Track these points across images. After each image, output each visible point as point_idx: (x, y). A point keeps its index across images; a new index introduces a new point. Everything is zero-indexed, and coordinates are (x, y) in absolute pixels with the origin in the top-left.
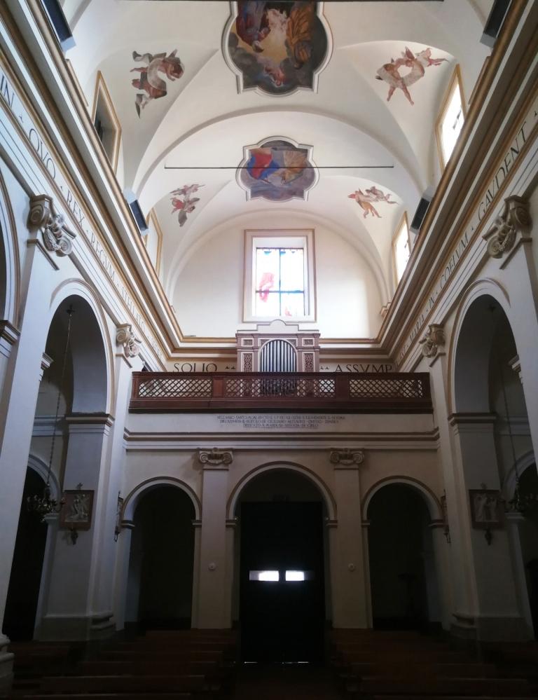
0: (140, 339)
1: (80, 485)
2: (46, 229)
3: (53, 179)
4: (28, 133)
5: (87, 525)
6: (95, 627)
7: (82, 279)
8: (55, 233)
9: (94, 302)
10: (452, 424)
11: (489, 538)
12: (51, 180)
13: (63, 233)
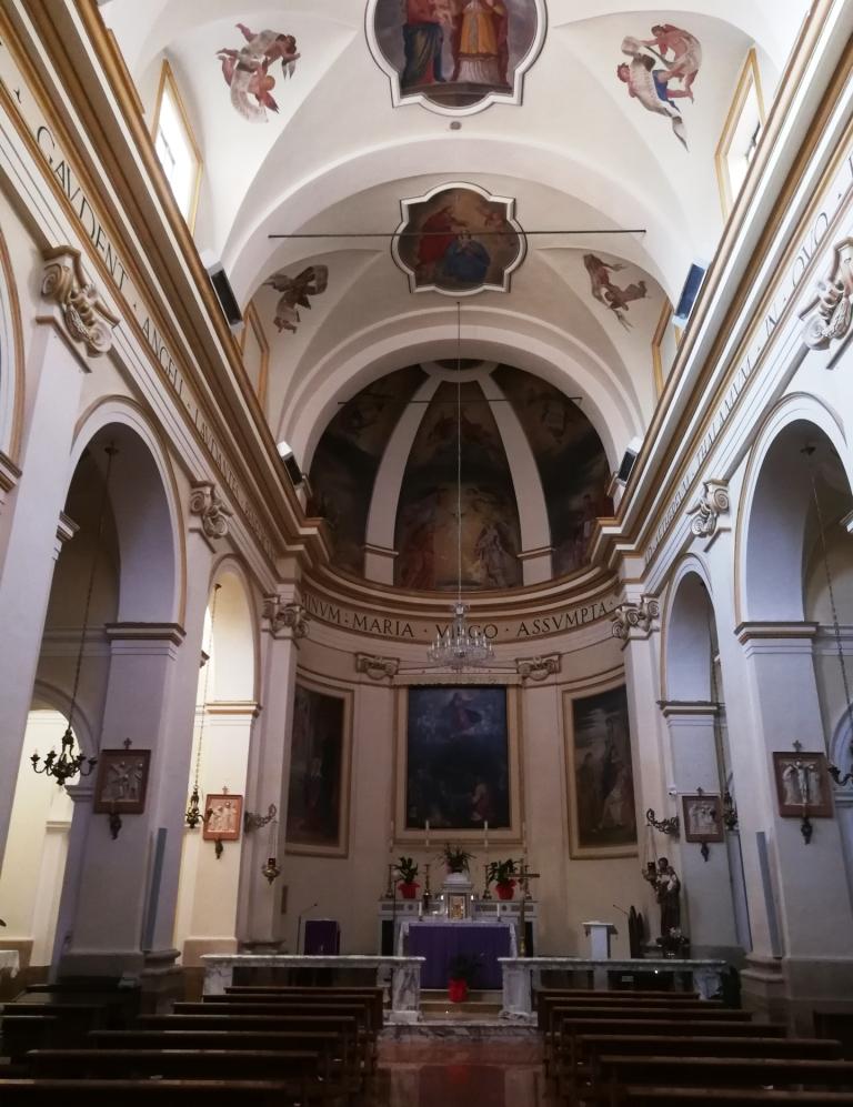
0: (230, 508)
1: (128, 742)
2: (68, 305)
3: (179, 396)
4: (35, 133)
5: (138, 808)
6: (150, 971)
7: (131, 396)
8: (83, 315)
9: (156, 444)
10: (743, 640)
11: (808, 832)
12: (75, 219)
13: (96, 316)
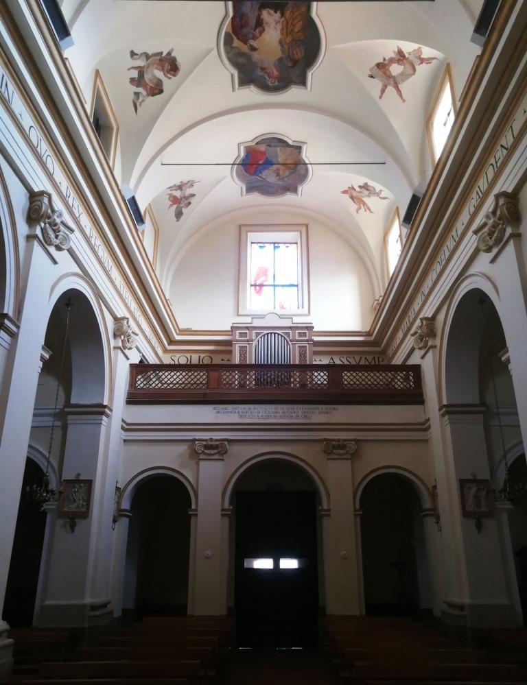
0: (138, 331)
1: (79, 475)
2: (45, 224)
3: (52, 175)
4: (27, 130)
5: (85, 514)
6: (93, 613)
7: (80, 273)
8: (54, 228)
9: (92, 295)
10: (443, 415)
11: (479, 526)
12: (50, 176)
13: (62, 228)
